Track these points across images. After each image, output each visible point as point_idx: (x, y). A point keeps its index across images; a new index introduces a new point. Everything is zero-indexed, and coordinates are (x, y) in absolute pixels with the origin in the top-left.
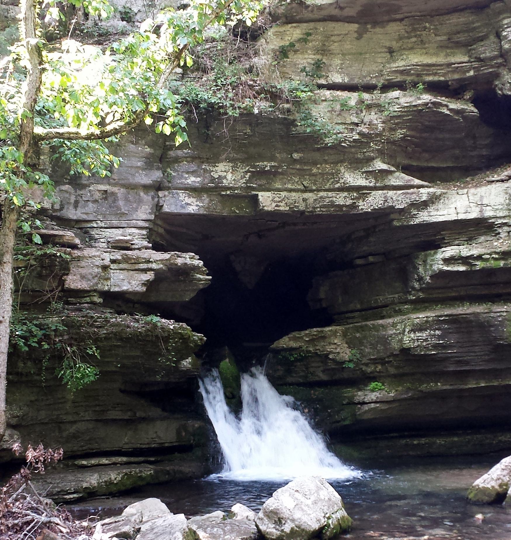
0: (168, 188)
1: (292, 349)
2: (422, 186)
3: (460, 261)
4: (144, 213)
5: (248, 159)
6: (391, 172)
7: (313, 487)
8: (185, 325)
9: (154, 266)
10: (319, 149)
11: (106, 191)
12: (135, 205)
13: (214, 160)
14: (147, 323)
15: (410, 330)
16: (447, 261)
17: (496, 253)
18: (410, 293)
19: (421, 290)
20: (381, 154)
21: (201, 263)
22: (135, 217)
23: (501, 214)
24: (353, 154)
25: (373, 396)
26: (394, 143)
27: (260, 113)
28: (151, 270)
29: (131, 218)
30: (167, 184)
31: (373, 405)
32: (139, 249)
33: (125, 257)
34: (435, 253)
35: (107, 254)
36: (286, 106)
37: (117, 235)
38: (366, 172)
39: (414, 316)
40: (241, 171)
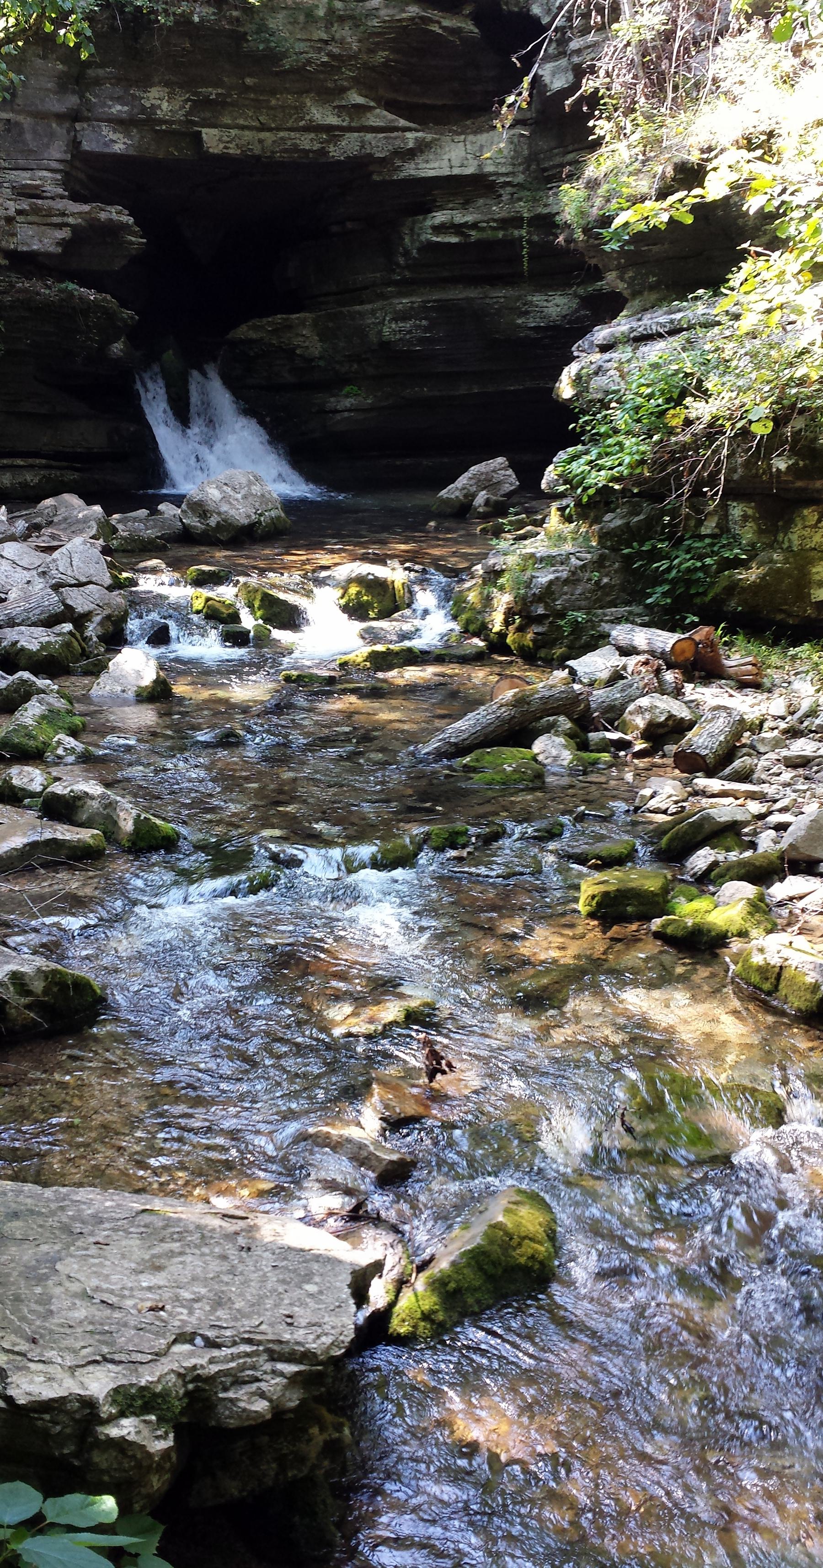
0: (88, 120)
1: (251, 341)
4: (57, 151)
5: (188, 84)
6: (369, 109)
7: (244, 481)
8: (109, 297)
9: (71, 220)
10: (277, 74)
11: (9, 120)
13: (146, 83)
14: (61, 291)
15: (394, 320)
16: (438, 229)
17: (494, 220)
18: (393, 271)
19: (407, 267)
20: (358, 83)
21: (131, 220)
22: (46, 155)
23: (503, 170)
24: (320, 81)
25: (348, 403)
26: (373, 69)
27: (202, 20)
28: (67, 225)
30: (86, 113)
31: (346, 414)
32: (52, 198)
34: (425, 219)
36: (235, 13)
37: (25, 178)
39: (396, 301)
40: (180, 99)
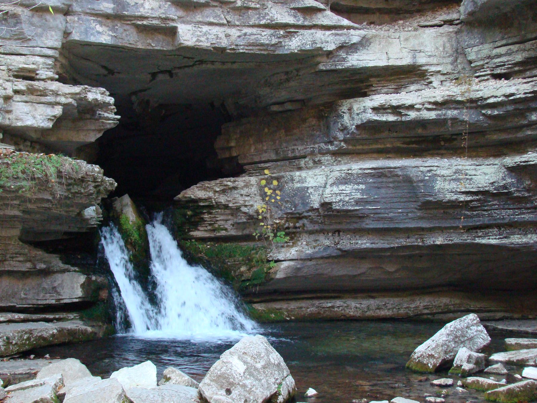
2: (349, 28)
3: (389, 111)
4: (54, 40)
6: (320, 10)
9: (63, 100)
12: (40, 30)
15: (323, 181)
17: (430, 103)
19: (345, 141)
21: (112, 100)
23: (434, 61)
28: (58, 104)
29: (35, 45)
32: (43, 80)
33: (30, 87)
35: (9, 84)
37: (18, 62)
38: (294, 9)
